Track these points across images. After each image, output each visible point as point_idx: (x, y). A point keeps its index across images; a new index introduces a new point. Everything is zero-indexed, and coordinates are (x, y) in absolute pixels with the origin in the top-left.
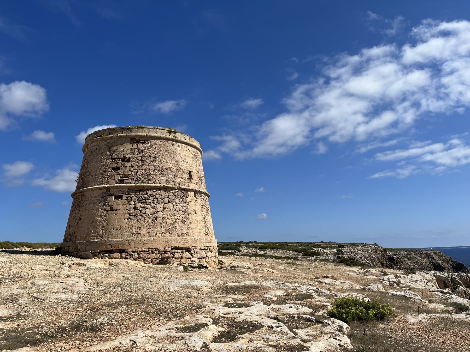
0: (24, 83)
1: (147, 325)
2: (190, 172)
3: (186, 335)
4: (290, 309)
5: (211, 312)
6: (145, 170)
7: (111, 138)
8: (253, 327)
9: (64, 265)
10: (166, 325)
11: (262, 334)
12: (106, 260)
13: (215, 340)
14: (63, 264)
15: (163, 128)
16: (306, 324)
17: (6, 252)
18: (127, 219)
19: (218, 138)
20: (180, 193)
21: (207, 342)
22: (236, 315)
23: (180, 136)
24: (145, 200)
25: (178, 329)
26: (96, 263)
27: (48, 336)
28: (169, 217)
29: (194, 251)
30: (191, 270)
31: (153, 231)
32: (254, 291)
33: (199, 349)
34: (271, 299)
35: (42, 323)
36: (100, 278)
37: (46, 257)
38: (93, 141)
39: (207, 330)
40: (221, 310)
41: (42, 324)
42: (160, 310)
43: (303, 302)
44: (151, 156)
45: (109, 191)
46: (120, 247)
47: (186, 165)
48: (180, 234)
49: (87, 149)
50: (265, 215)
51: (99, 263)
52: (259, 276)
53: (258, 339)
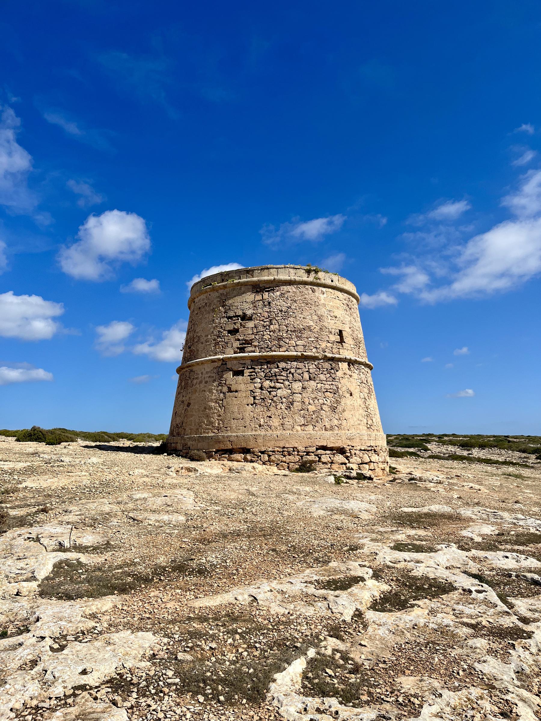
0: (116, 212)
1: (274, 572)
2: (341, 331)
3: (330, 594)
4: (503, 560)
5: (371, 558)
6: (274, 331)
7: (225, 287)
8: (438, 589)
9: (170, 470)
10: (301, 575)
11: (453, 602)
12: (225, 462)
13: (376, 606)
14: (169, 468)
15: (299, 267)
16: (530, 590)
17: (100, 448)
18: (252, 405)
19: (393, 271)
20: (327, 365)
21: (362, 608)
22: (411, 565)
23: (324, 277)
24: (276, 376)
25: (319, 583)
26: (211, 467)
27: (142, 579)
28: (311, 402)
29: (350, 453)
30: (347, 483)
31: (288, 422)
32: (444, 524)
33: (348, 619)
34: (472, 539)
35: (136, 558)
36: (215, 492)
37: (149, 457)
38: (201, 293)
39: (362, 588)
40: (387, 555)
41: (135, 560)
42: (295, 548)
43: (528, 548)
44: (281, 311)
45: (226, 364)
46: (244, 445)
47: (333, 322)
49: (193, 304)
50: (470, 391)
51: (215, 467)
52: (456, 496)
53: (445, 610)
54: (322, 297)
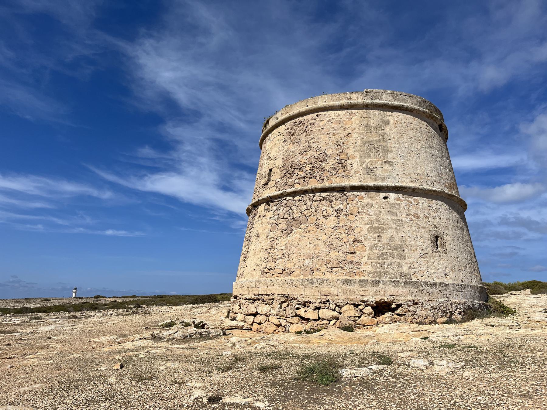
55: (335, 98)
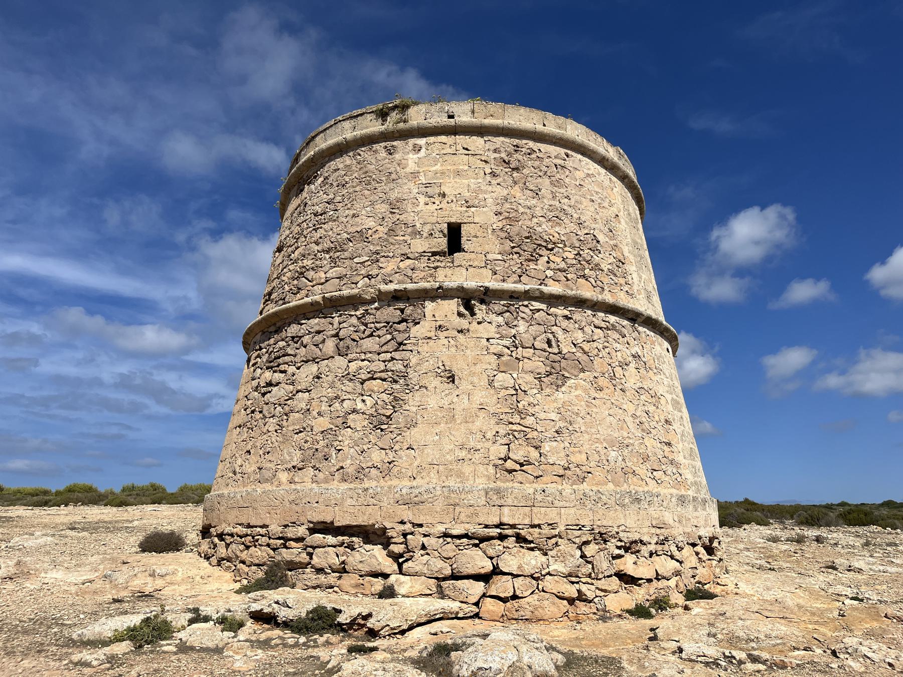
15: (360, 111)
20: (391, 313)
48: (351, 470)
54: (413, 157)
55: (591, 138)
